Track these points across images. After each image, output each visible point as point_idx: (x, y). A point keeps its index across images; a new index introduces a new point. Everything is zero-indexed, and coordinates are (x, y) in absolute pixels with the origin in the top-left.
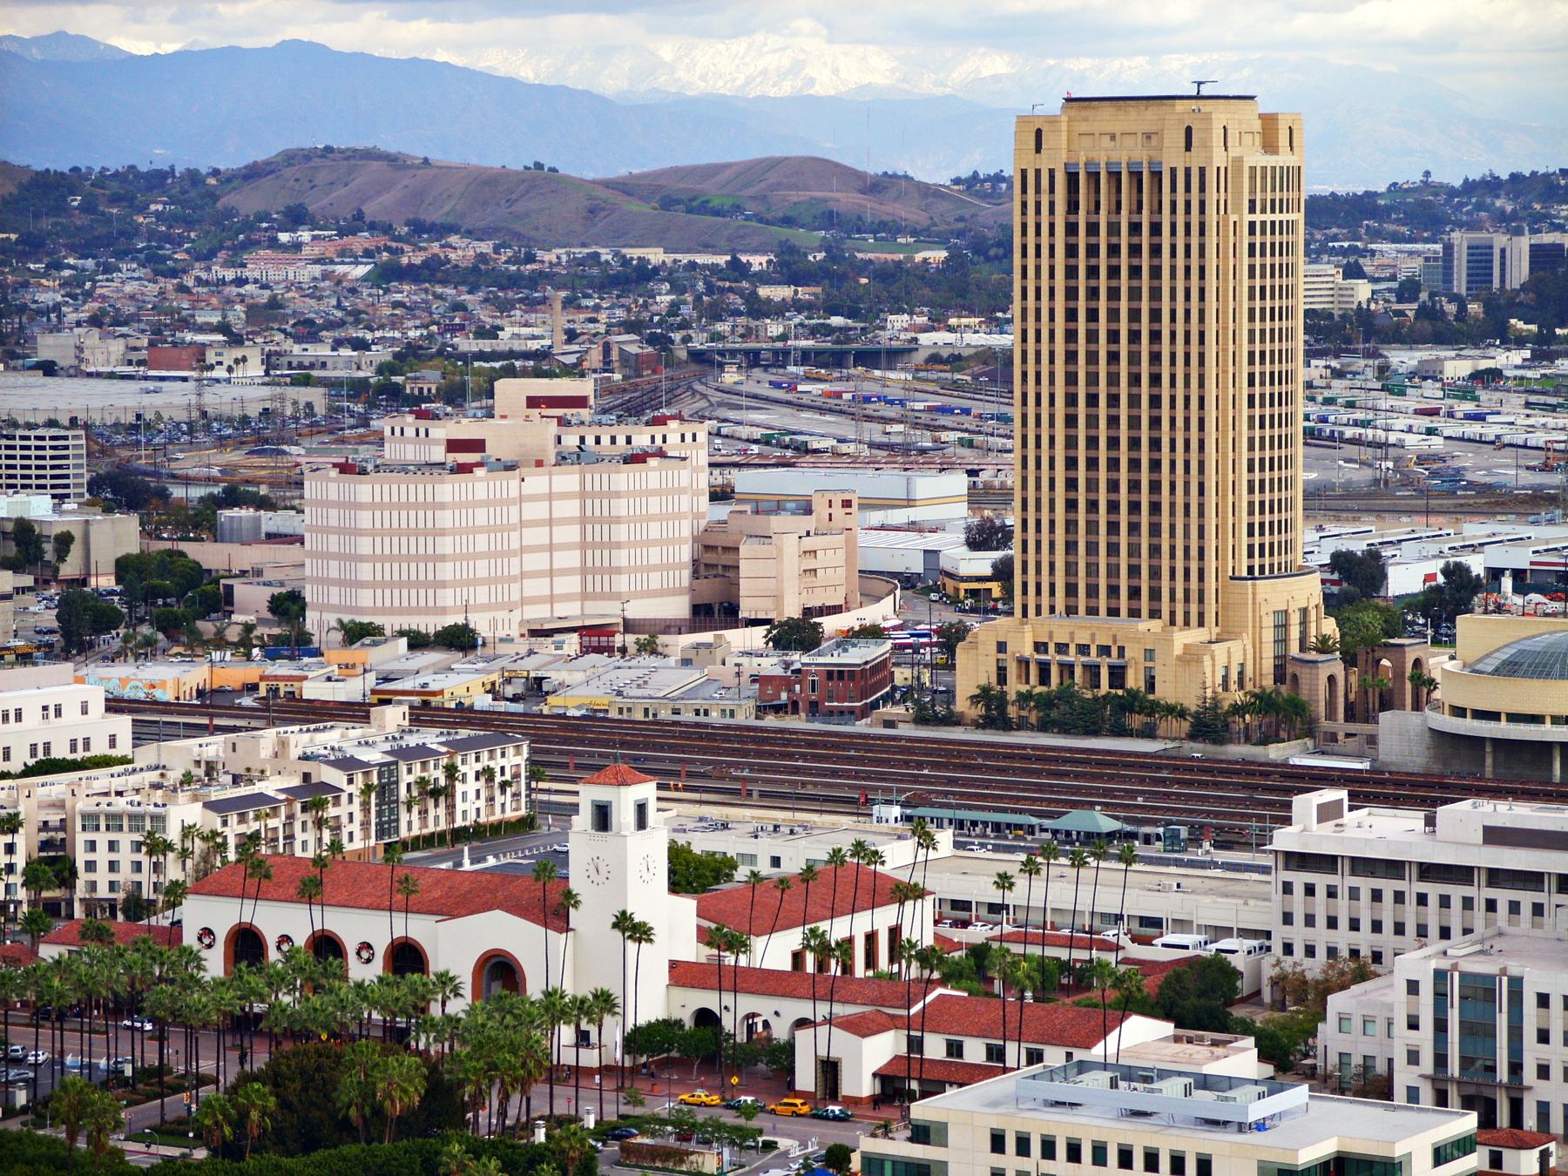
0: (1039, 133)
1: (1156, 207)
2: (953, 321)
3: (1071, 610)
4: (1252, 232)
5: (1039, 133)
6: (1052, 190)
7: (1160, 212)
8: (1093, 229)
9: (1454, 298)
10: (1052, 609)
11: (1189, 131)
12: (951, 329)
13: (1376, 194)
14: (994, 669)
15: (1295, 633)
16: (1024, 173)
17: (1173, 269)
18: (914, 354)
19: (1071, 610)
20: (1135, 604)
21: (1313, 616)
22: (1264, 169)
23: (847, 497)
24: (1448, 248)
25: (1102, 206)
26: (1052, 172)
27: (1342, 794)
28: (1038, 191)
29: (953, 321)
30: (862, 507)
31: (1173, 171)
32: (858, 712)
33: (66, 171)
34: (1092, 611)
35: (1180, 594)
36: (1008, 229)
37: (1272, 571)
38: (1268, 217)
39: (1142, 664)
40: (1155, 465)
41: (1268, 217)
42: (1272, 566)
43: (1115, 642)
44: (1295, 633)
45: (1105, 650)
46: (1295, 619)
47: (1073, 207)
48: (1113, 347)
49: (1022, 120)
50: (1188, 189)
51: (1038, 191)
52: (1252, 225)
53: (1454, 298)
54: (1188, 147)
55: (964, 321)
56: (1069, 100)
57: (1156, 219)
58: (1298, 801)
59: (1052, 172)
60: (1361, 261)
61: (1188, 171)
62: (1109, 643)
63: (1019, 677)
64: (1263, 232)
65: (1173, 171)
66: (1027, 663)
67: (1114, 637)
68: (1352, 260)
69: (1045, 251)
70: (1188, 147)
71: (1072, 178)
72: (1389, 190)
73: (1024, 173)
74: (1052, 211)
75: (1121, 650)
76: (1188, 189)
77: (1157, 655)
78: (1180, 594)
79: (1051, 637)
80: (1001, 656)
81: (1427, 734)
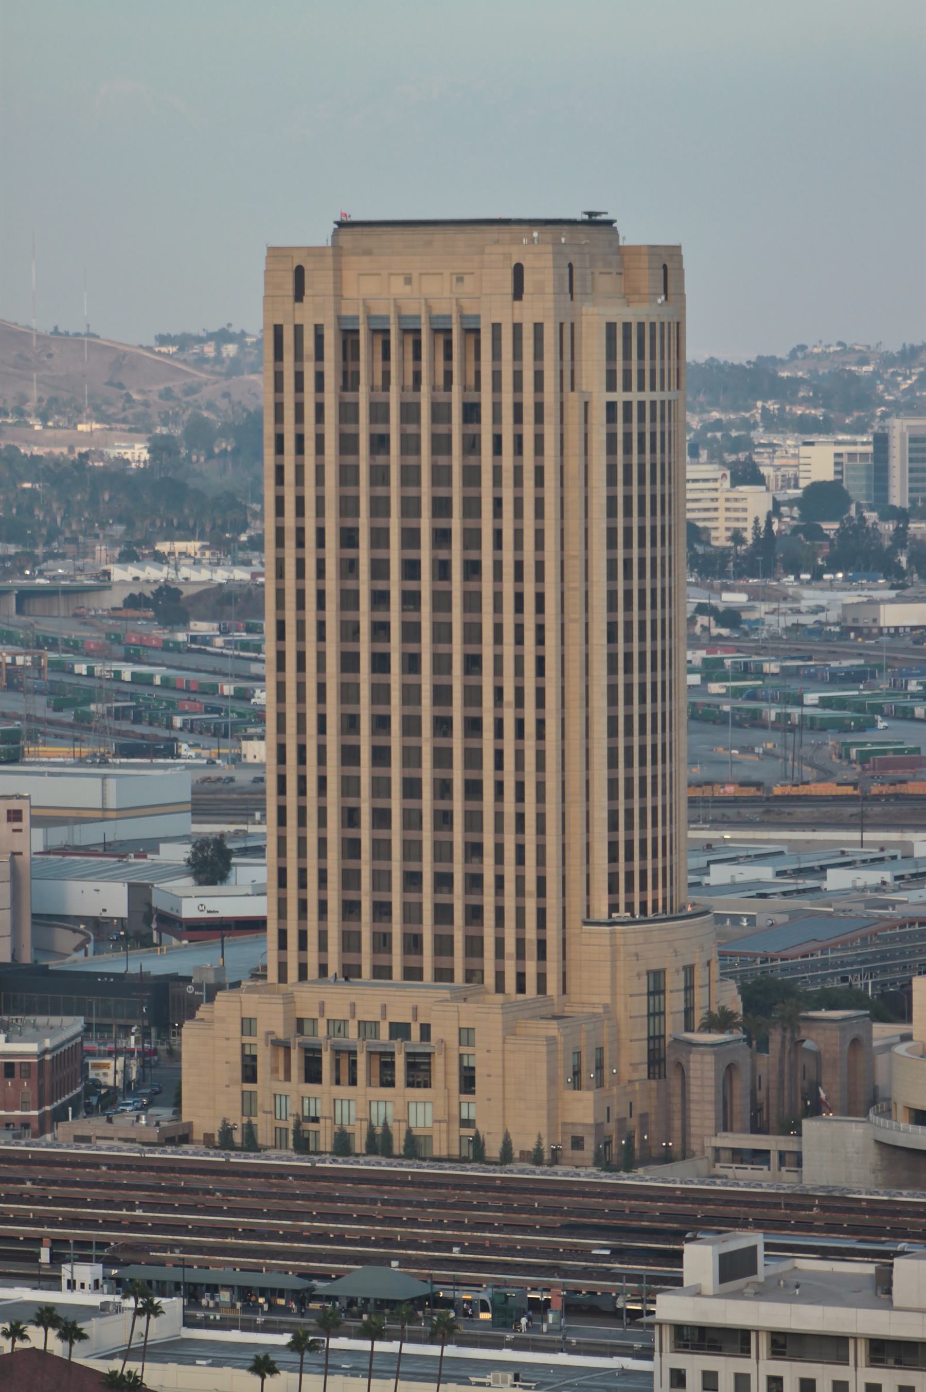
0: (299, 272)
1: (471, 380)
2: (163, 547)
3: (350, 972)
4: (611, 417)
5: (299, 272)
6: (319, 355)
7: (478, 387)
8: (379, 413)
9: (889, 513)
10: (323, 969)
11: (518, 271)
12: (160, 559)
13: (773, 360)
14: (238, 1059)
15: (674, 1002)
16: (278, 331)
17: (497, 471)
18: (106, 594)
19: (350, 972)
20: (444, 962)
21: (700, 977)
22: (627, 326)
23: (15, 805)
24: (882, 442)
25: (393, 380)
26: (538, 328)
27: (755, 1239)
28: (299, 356)
29: (163, 547)
30: (36, 822)
31: (496, 328)
32: (35, 1125)
33: (744, 363)
34: (382, 972)
35: (510, 947)
36: (256, 419)
37: (643, 911)
38: (634, 396)
39: (454, 1049)
40: (350, 723)
41: (634, 396)
42: (643, 905)
43: (415, 1017)
44: (674, 1002)
45: (400, 1030)
46: (674, 982)
47: (349, 381)
48: (411, 585)
49: (275, 254)
50: (517, 355)
51: (299, 356)
52: (611, 407)
53: (889, 513)
54: (518, 293)
55: (180, 546)
56: (341, 224)
57: (472, 397)
58: (691, 1251)
59: (538, 328)
60: (756, 459)
61: (517, 328)
62: (407, 1019)
63: (275, 1070)
64: (627, 419)
65: (496, 328)
66: (287, 1049)
67: (415, 1009)
68: (742, 456)
69: (310, 445)
70: (518, 293)
71: (348, 337)
72: (793, 355)
73: (278, 331)
74: (320, 386)
75: (426, 1030)
76: (517, 355)
77: (478, 1037)
78: (510, 947)
79: (322, 1012)
80: (247, 1040)
81: (873, 1151)
